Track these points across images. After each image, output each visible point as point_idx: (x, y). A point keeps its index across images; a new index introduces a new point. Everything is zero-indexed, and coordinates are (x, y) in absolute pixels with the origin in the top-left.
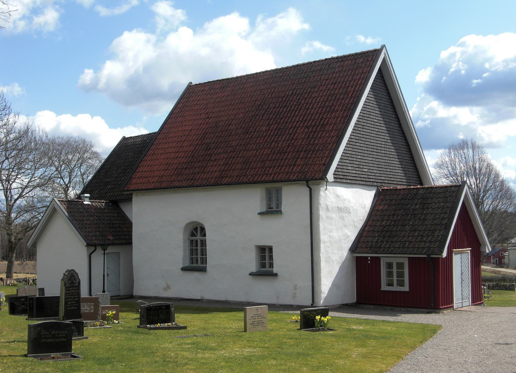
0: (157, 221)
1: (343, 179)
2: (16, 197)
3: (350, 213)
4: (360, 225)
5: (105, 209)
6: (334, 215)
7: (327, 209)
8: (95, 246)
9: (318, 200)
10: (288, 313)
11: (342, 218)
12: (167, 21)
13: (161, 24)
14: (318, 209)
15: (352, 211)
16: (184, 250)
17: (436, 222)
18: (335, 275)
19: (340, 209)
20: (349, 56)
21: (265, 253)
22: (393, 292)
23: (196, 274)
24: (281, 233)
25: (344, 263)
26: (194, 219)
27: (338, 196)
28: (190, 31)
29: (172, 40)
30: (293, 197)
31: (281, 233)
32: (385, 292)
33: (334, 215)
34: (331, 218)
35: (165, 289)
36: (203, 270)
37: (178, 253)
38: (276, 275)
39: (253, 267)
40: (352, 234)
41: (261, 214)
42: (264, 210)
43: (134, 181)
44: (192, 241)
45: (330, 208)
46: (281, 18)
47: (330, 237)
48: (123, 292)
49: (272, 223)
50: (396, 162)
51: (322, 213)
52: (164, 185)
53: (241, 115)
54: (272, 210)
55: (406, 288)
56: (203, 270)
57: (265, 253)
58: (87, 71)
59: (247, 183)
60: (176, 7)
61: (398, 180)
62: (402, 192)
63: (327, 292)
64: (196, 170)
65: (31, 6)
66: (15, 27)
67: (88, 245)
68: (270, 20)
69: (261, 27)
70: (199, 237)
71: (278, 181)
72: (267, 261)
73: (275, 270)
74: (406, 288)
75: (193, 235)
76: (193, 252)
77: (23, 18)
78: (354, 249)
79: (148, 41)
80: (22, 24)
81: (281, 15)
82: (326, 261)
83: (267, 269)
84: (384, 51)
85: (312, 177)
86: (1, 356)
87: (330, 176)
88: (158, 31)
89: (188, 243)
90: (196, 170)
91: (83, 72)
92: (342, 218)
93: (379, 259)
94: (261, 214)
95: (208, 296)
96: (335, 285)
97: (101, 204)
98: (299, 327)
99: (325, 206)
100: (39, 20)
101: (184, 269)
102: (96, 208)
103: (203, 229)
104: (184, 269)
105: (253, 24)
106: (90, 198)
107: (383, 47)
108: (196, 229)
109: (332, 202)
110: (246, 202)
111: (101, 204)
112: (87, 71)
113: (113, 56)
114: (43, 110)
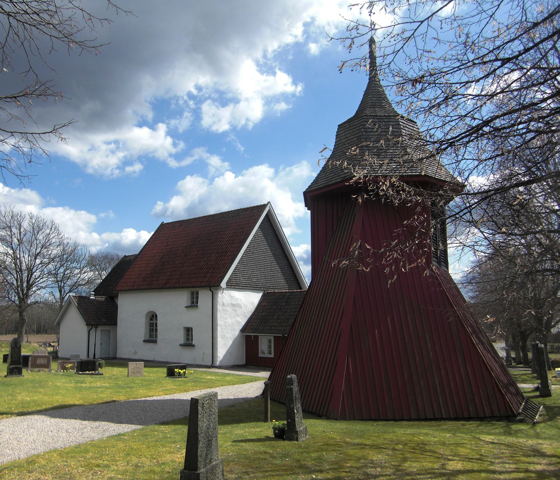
0: (132, 309)
1: (233, 285)
2: (67, 292)
3: (241, 307)
4: (249, 315)
5: (104, 302)
6: (228, 309)
7: (223, 305)
8: (92, 325)
9: (217, 299)
10: (209, 372)
11: (236, 311)
12: (217, 169)
13: (212, 171)
14: (217, 306)
15: (242, 306)
16: (145, 329)
17: (291, 314)
18: (229, 346)
19: (233, 305)
20: (250, 208)
21: (189, 331)
22: (265, 358)
23: (151, 345)
24: (196, 319)
25: (235, 339)
26: (151, 310)
27: (232, 297)
28: (234, 175)
29: (219, 181)
30: (204, 296)
31: (196, 319)
32: (260, 357)
33: (228, 309)
34: (226, 311)
35: (134, 354)
36: (155, 342)
37: (142, 332)
38: (194, 346)
39: (182, 341)
40: (243, 321)
41: (187, 307)
42: (189, 305)
43: (119, 285)
44: (150, 324)
45: (225, 304)
46: (296, 167)
47: (225, 322)
48: (111, 356)
49: (193, 313)
50: (280, 275)
51: (219, 307)
52: (135, 288)
53: (186, 244)
54: (194, 304)
55: (272, 356)
56: (155, 342)
57: (189, 331)
58: (159, 203)
59: (178, 288)
60: (224, 161)
61: (281, 286)
62: (288, 294)
63: (222, 357)
64: (154, 279)
65: (123, 160)
66: (112, 174)
67: (87, 325)
68: (288, 169)
69: (282, 174)
70: (154, 321)
71: (197, 287)
72: (190, 337)
73: (194, 343)
74: (272, 356)
75: (151, 319)
76: (151, 330)
77: (118, 168)
78: (243, 330)
79: (203, 182)
80: (117, 172)
81: (295, 166)
82: (222, 338)
83: (190, 342)
84: (269, 205)
85: (213, 285)
86: (559, 429)
87: (223, 284)
88: (210, 176)
89: (148, 325)
90: (154, 279)
91: (156, 203)
92: (236, 311)
93: (258, 336)
94: (187, 307)
95: (157, 359)
96: (228, 353)
97: (102, 298)
98: (5, 374)
99: (222, 303)
100: (129, 169)
101: (145, 341)
102: (98, 301)
103: (156, 316)
104: (145, 341)
105: (277, 173)
106: (95, 295)
107: (269, 202)
108: (153, 316)
109: (227, 301)
110: (181, 298)
111: (102, 298)
112: (159, 203)
113: (178, 193)
114: (129, 228)
